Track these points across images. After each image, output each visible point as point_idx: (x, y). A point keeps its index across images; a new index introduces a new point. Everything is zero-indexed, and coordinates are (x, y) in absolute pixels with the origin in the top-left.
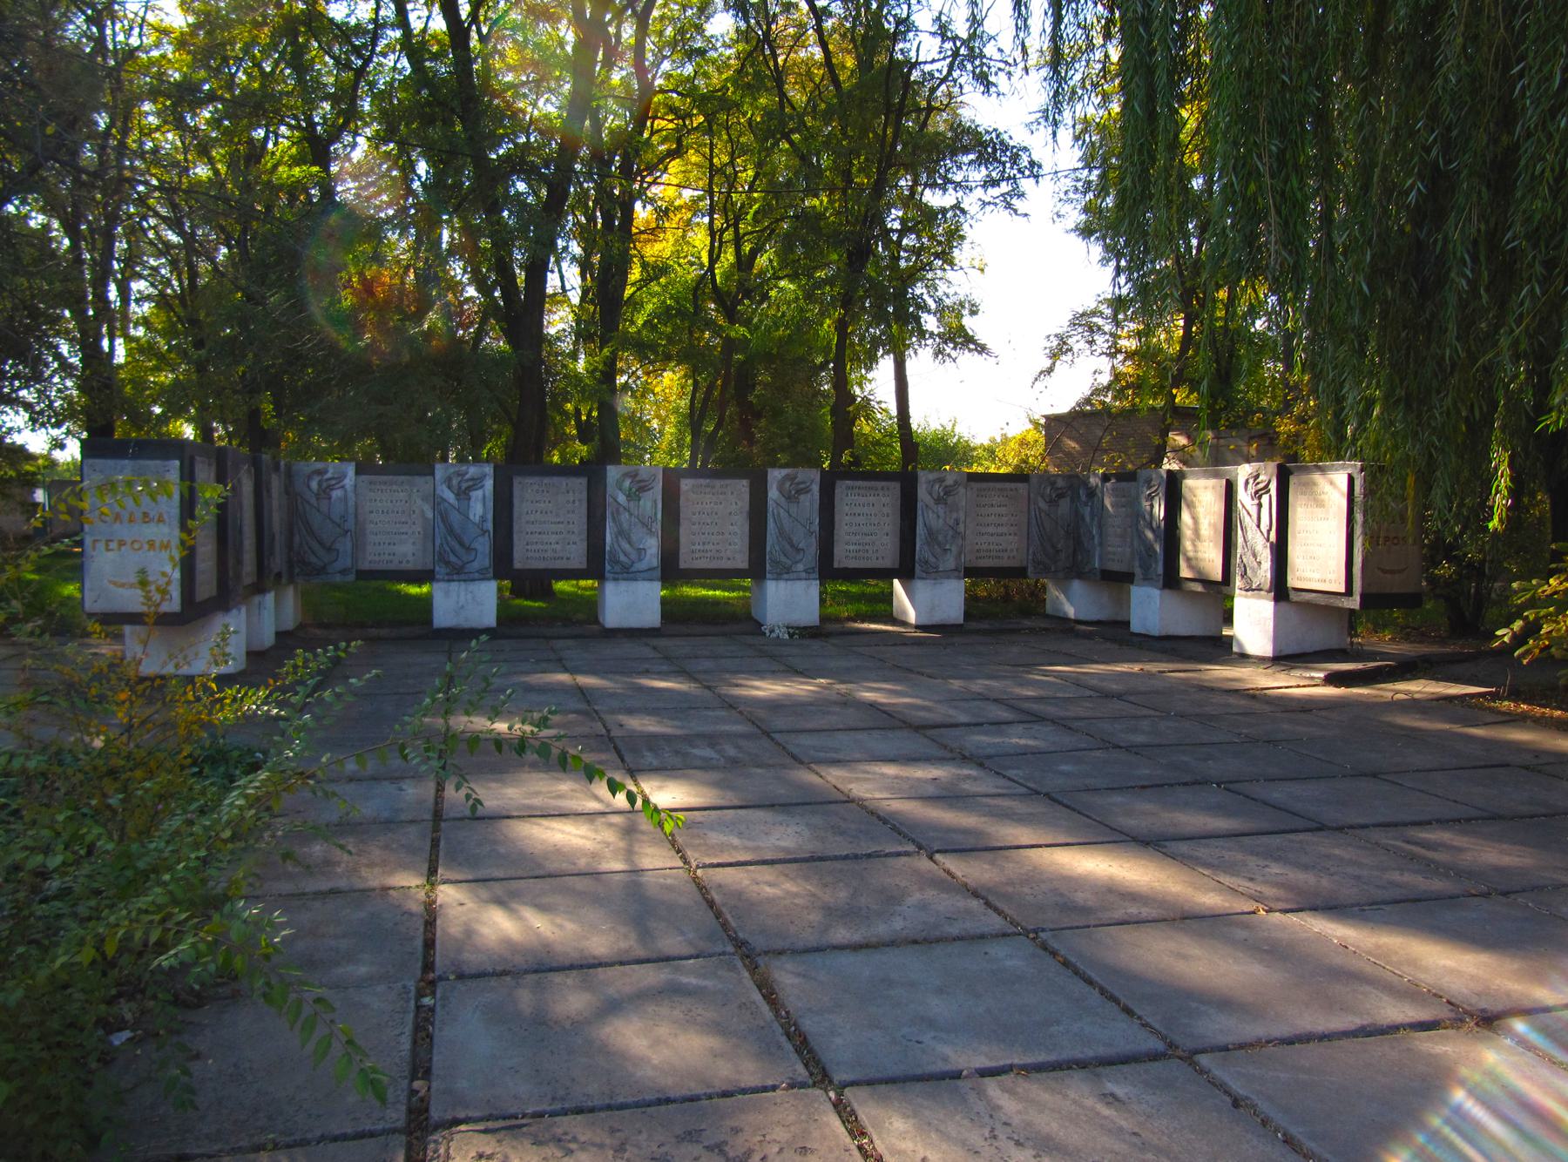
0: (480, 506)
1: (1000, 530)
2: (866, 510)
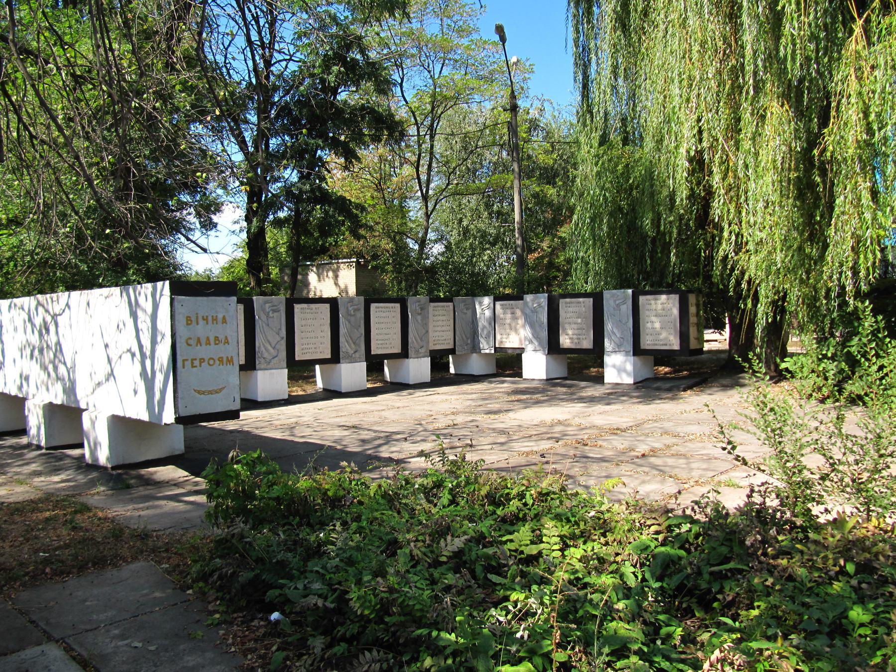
1: (444, 328)
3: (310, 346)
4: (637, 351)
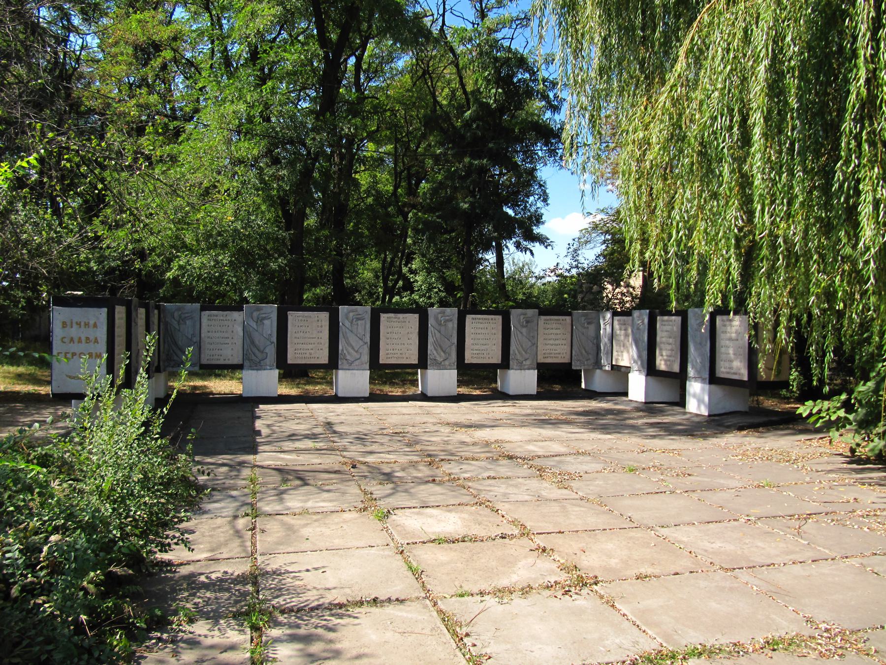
0: (270, 326)
1: (557, 342)
2: (483, 331)
3: (395, 352)
4: (713, 379)
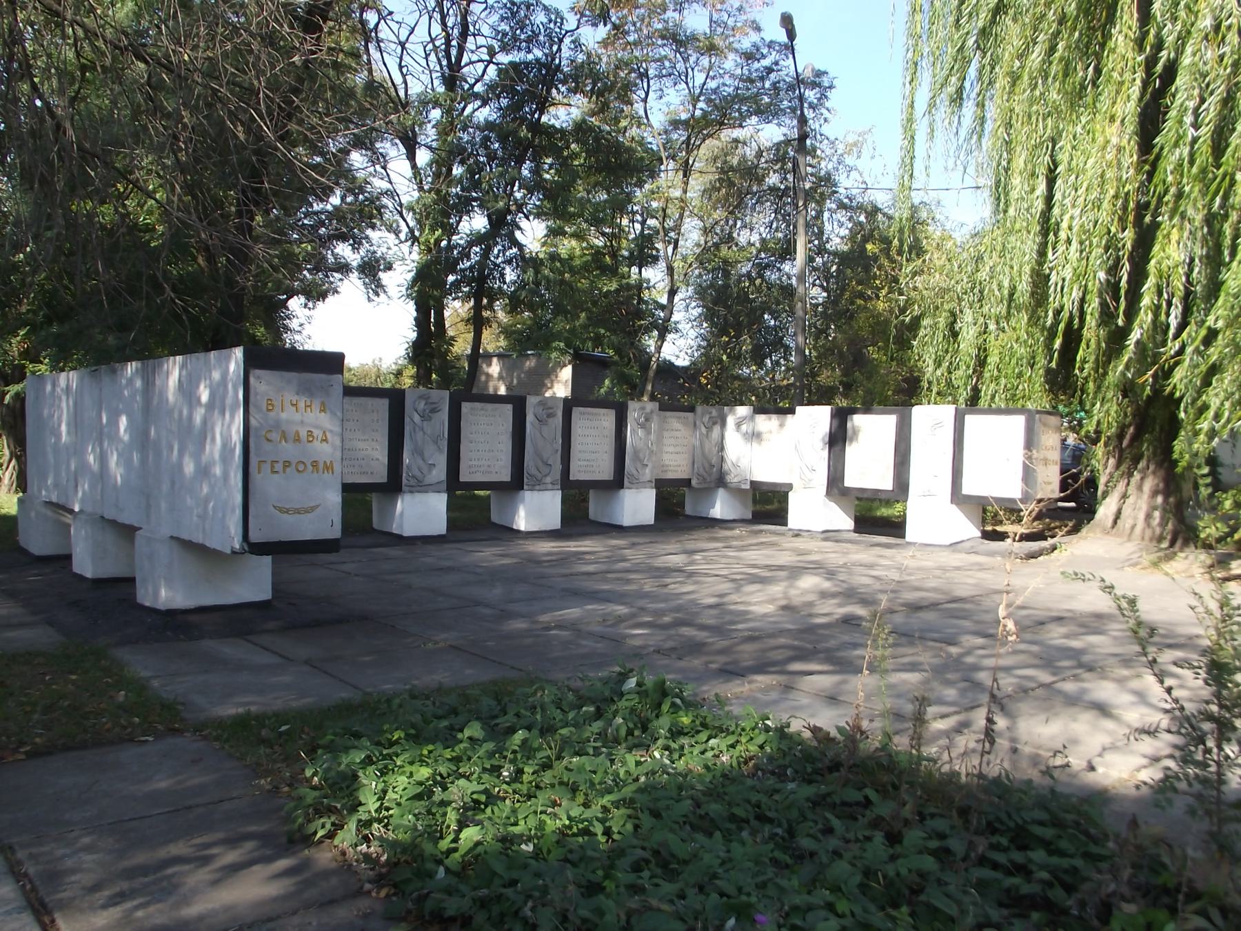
3: (480, 463)
